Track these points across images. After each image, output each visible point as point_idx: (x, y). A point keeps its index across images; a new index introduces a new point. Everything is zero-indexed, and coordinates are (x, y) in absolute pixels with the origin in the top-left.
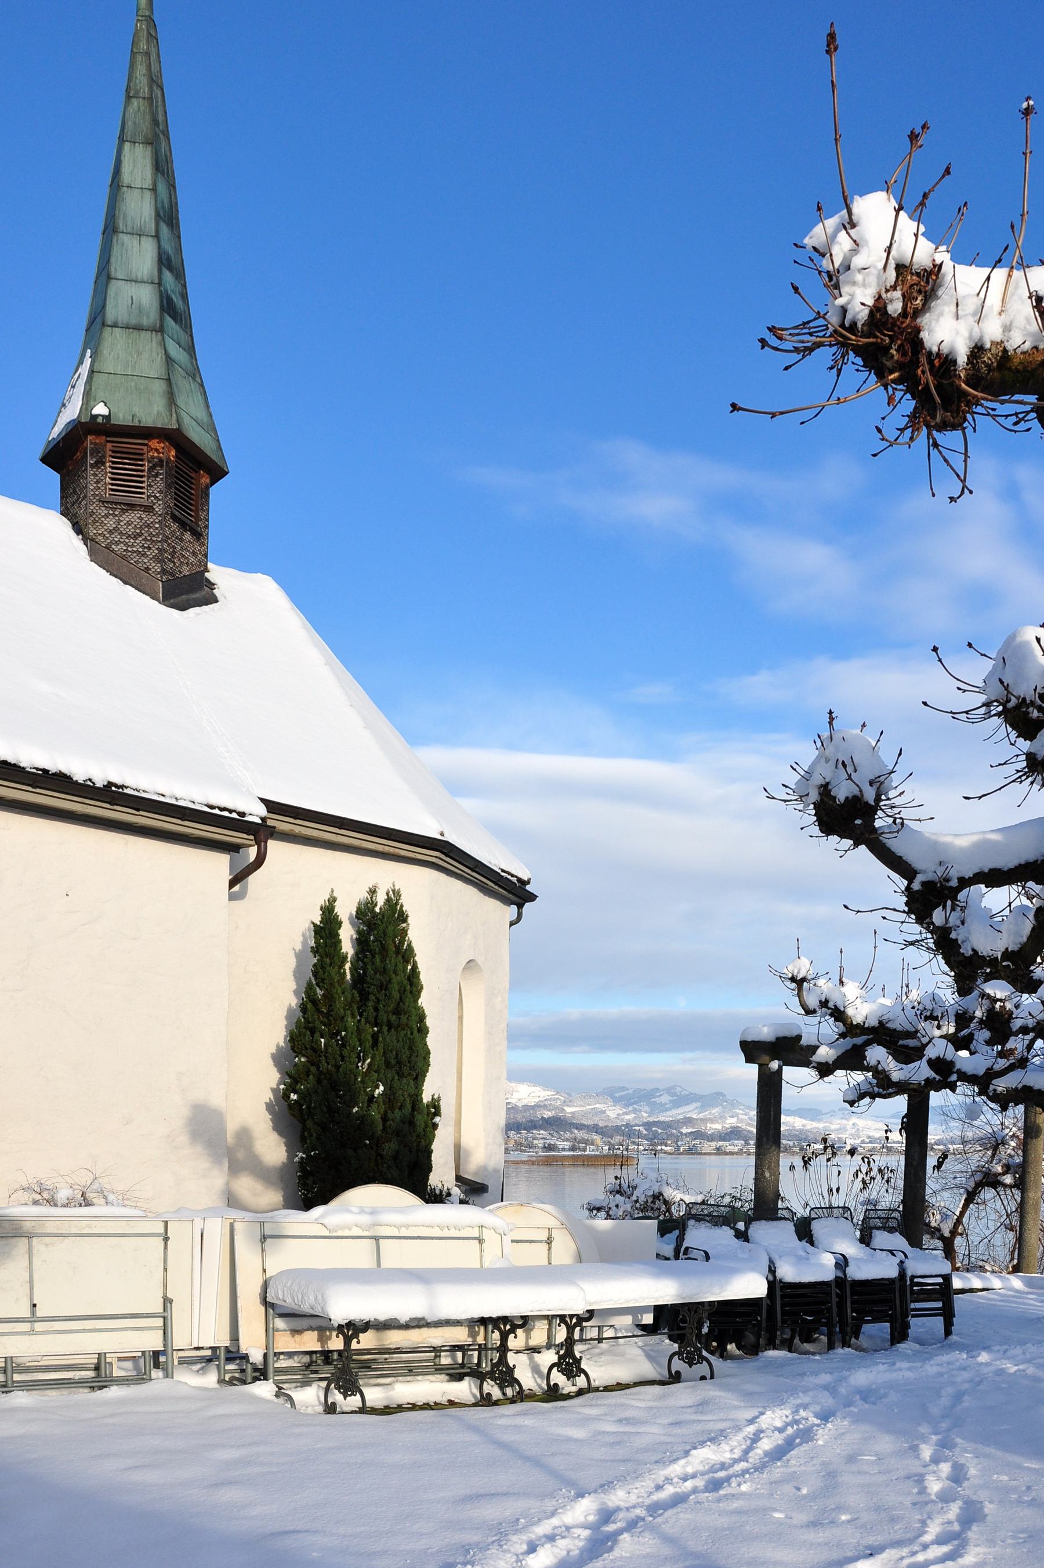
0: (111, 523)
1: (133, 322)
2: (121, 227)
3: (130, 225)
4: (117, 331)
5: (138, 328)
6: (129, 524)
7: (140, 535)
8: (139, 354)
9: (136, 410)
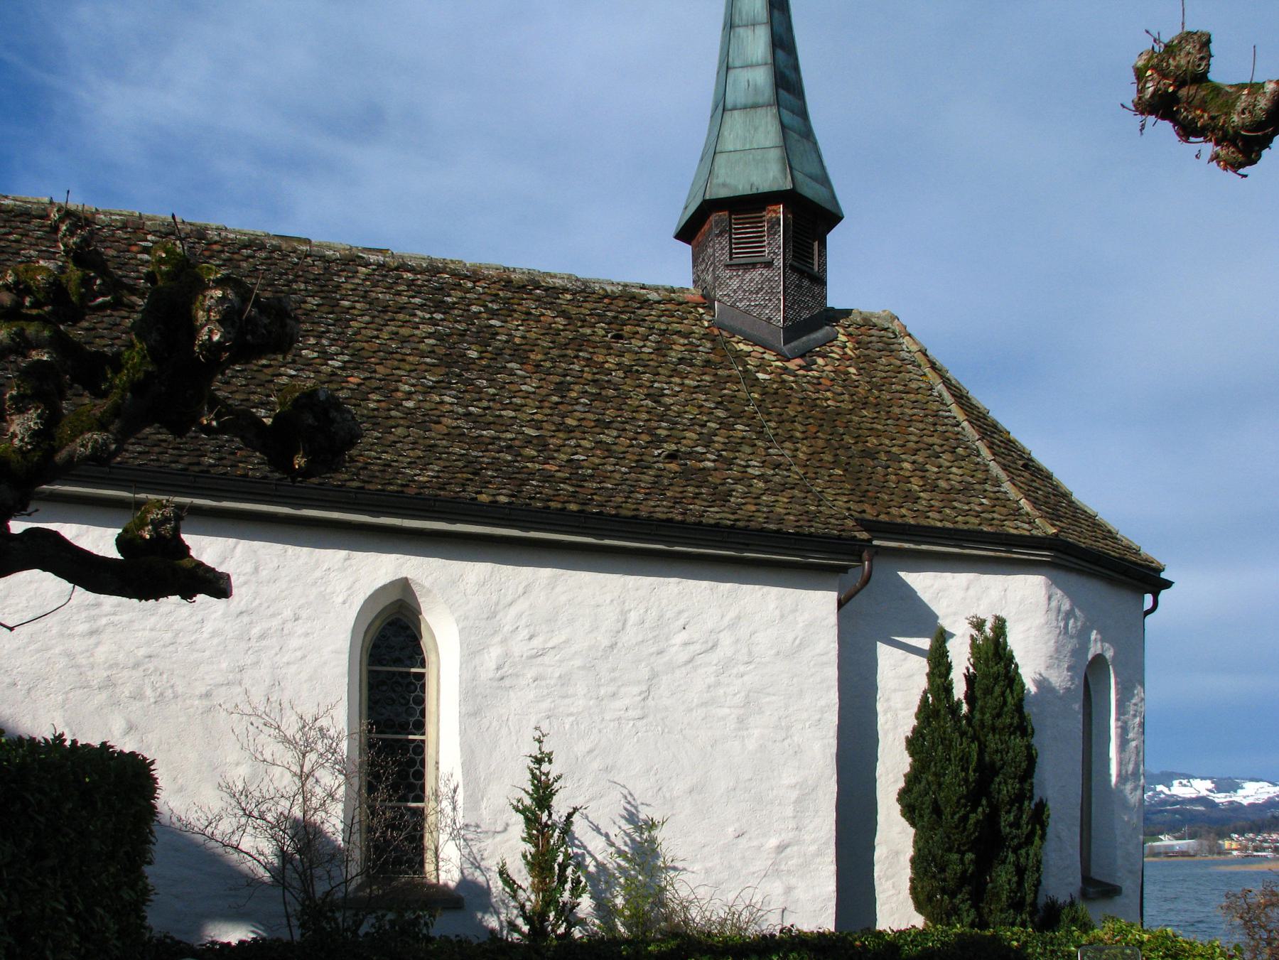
0: (735, 283)
1: (750, 101)
2: (770, 66)
3: (744, 17)
4: (736, 113)
5: (755, 106)
6: (751, 280)
7: (761, 289)
8: (756, 129)
9: (239, 774)
